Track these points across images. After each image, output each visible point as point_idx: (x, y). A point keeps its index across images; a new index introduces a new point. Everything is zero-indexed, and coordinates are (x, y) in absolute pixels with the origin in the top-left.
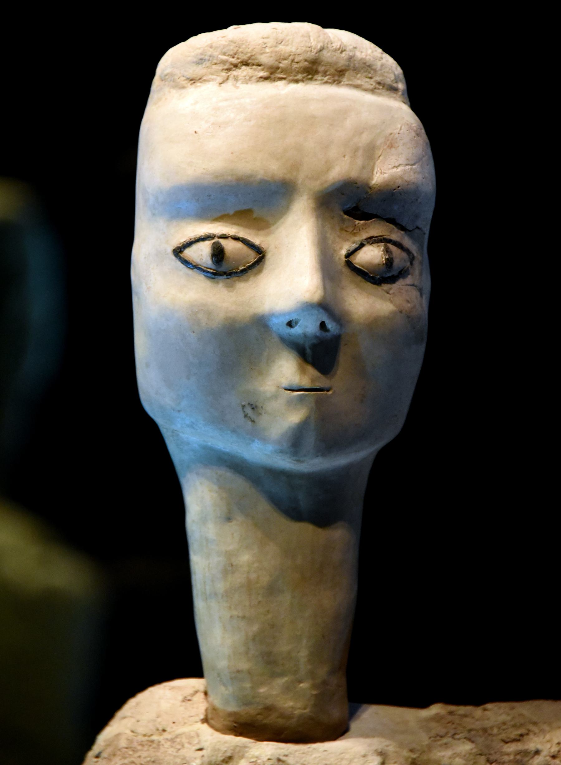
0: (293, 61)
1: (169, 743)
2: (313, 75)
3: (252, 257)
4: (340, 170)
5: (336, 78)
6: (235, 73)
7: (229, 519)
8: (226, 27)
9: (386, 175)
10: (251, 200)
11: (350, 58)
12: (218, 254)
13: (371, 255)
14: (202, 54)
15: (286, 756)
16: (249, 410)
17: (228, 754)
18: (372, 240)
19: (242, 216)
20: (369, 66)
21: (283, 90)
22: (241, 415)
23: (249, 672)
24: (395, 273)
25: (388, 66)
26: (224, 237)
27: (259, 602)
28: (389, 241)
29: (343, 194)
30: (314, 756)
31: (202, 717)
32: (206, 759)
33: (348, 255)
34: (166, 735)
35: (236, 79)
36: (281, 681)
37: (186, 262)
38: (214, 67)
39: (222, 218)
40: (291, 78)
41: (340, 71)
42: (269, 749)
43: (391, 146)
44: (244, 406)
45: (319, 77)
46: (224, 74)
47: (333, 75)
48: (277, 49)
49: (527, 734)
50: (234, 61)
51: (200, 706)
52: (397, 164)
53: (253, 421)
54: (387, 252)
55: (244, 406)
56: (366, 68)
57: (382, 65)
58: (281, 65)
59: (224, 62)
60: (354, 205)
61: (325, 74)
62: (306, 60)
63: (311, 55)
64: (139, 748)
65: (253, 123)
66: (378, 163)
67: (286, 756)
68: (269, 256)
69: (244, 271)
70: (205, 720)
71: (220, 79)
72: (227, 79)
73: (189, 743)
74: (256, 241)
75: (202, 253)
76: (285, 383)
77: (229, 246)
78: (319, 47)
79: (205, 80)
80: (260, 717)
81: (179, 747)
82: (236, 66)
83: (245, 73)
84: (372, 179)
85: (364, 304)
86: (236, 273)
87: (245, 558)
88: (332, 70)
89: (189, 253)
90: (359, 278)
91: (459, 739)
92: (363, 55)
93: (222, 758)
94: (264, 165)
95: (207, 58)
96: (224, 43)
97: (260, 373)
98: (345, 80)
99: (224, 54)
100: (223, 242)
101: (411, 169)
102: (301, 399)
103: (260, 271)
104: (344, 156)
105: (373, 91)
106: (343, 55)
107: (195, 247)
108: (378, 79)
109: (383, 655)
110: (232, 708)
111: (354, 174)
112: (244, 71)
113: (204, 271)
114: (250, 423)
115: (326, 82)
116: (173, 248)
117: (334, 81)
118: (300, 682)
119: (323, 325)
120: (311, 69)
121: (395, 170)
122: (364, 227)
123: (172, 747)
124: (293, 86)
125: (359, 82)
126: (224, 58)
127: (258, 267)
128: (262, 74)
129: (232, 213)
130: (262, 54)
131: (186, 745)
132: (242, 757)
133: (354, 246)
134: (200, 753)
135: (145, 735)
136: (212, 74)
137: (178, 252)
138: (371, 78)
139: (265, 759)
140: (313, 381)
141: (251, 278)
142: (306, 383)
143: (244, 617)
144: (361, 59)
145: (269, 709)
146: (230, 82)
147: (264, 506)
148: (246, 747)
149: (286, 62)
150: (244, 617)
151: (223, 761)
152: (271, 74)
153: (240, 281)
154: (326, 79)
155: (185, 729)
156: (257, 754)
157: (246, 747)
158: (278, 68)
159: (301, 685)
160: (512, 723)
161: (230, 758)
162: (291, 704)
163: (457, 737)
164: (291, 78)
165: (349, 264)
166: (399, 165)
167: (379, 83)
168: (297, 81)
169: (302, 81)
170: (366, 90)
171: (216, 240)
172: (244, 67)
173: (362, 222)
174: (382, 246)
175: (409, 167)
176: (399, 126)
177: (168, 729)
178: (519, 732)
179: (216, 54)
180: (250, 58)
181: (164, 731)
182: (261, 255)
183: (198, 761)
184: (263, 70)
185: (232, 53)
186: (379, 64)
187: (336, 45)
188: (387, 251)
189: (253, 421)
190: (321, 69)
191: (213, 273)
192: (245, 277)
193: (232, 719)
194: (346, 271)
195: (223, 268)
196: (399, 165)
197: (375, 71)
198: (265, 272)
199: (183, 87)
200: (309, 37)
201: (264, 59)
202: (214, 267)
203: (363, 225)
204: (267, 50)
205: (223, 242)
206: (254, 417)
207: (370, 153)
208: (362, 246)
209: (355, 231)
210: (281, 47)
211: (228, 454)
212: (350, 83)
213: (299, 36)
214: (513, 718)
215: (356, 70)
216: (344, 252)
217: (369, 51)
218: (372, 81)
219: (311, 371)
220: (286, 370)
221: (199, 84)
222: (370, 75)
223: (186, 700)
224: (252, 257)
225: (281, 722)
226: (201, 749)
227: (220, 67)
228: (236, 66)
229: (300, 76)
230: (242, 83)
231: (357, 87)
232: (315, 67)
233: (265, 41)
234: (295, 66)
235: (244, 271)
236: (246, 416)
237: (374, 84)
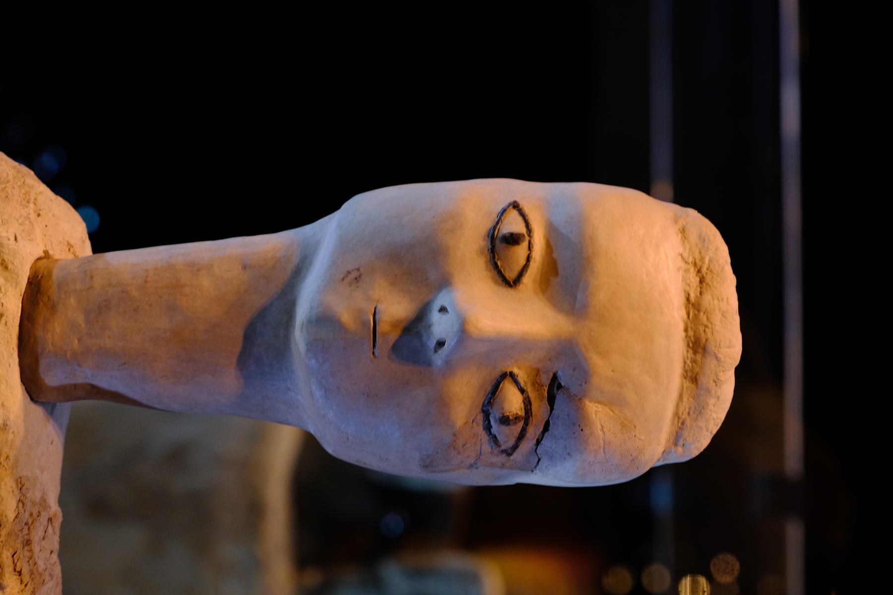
0: (706, 326)
1: (25, 214)
2: (692, 348)
3: (511, 275)
4: (598, 364)
5: (689, 374)
6: (692, 270)
7: (245, 267)
8: (736, 271)
9: (594, 416)
10: (567, 275)
11: (708, 391)
12: (513, 240)
13: (512, 401)
14: (709, 240)
15: (6, 324)
16: (354, 275)
17: (10, 267)
18: (527, 403)
19: (552, 267)
20: (700, 412)
21: (676, 315)
22: (350, 268)
23: (91, 287)
24: (495, 428)
25: (699, 441)
26: (530, 248)
27: (161, 297)
28: (526, 424)
29: (574, 370)
30: (4, 352)
31: (51, 252)
32: (5, 242)
33: (512, 375)
34: (33, 216)
35: (687, 271)
36: (80, 319)
37: (508, 206)
38: (697, 252)
39: (549, 247)
40: (689, 324)
41: (696, 379)
42: (14, 307)
43: (623, 426)
44: (358, 270)
45: (690, 354)
46: (691, 260)
47: (692, 371)
48: (717, 311)
49: (22, 582)
50: (704, 270)
51: (59, 253)
52: (605, 430)
53: (343, 279)
54: (516, 418)
55: (358, 270)
56: (699, 410)
57: (701, 428)
58: (702, 314)
59: (702, 260)
60: (563, 384)
61: (694, 361)
62: (707, 340)
63: (711, 346)
64: (23, 191)
65: (644, 277)
66: (607, 409)
67: (6, 324)
68: (510, 292)
69: (496, 266)
70: (47, 255)
71: (686, 255)
72: (686, 263)
73: (23, 231)
74: (527, 279)
75: (513, 224)
76: (381, 307)
77: (521, 251)
78: (719, 355)
79: (684, 242)
80: (45, 299)
81: (20, 221)
82: (699, 271)
83: (692, 279)
84: (590, 402)
85: (464, 391)
86: (494, 257)
87: (206, 282)
88: (697, 370)
89: (513, 214)
90: (489, 388)
91: (17, 507)
92: (711, 407)
93: (6, 259)
94: (603, 287)
95: (706, 245)
96: (721, 261)
97: (393, 284)
98: (687, 384)
99: (710, 261)
100: (525, 244)
101: (600, 447)
102: (365, 324)
103: (496, 283)
104: (613, 371)
105: (676, 414)
106: (712, 383)
107: (520, 219)
108: (688, 422)
109: (124, 485)
110: (56, 274)
111: (595, 380)
112: (694, 280)
113: (498, 223)
114: (342, 276)
115: (685, 363)
116: (518, 201)
117: (686, 372)
118: (79, 340)
119: (441, 344)
120: (698, 345)
121: (599, 427)
122: (540, 396)
123: (21, 216)
124: (681, 326)
125: (685, 399)
126: (707, 260)
127: (500, 280)
128: (692, 296)
129: (555, 255)
130: (712, 296)
131: (22, 228)
132: (6, 280)
133: (522, 384)
134: (13, 238)
135: (35, 199)
136: (690, 249)
137: (515, 206)
138: (689, 414)
139: (3, 301)
140: (384, 334)
141: (489, 274)
142: (382, 328)
143: (146, 282)
144: (708, 404)
145: (53, 308)
146: (682, 264)
147: (258, 302)
148: (17, 284)
149: (705, 319)
150: (146, 282)
151: (3, 260)
152: (693, 304)
153: (486, 262)
154: (688, 362)
155: (38, 232)
156: (9, 294)
157: (17, 284)
158: (699, 311)
159: (76, 341)
160: (35, 571)
161: (6, 268)
162: (58, 330)
163: (21, 505)
164: (689, 324)
165: (504, 376)
166: (604, 433)
167: (683, 423)
168: (686, 330)
169: (686, 336)
170: (677, 406)
171: (527, 238)
172: (698, 279)
173: (546, 394)
174: (522, 413)
175: (602, 445)
176: (642, 438)
177: (40, 219)
178: (25, 571)
179: (710, 253)
180: (707, 284)
181: (39, 215)
182: (512, 283)
183: (4, 234)
184: (697, 297)
185: (712, 267)
186: (702, 424)
187: (722, 376)
188: (517, 418)
189: (343, 279)
190: (699, 357)
191: (493, 234)
192: (491, 267)
193: (45, 273)
194: (497, 373)
195: (499, 244)
196: (604, 433)
197: (696, 419)
198: (495, 288)
199: (676, 222)
200: (729, 348)
201: (707, 298)
202: (500, 235)
203: (543, 395)
204: (716, 301)
205: (525, 244)
206: (347, 280)
207: (615, 402)
208: (522, 391)
209: (537, 385)
210: (720, 315)
211: (311, 264)
212: (685, 390)
213: (729, 342)
214: (40, 574)
215: (696, 397)
216: (516, 371)
217: (714, 416)
218: (685, 416)
219: (394, 336)
220: (395, 308)
221: (680, 236)
222: (691, 413)
223: (70, 246)
224: (511, 275)
225: (41, 320)
226: (16, 239)
227: (697, 256)
228: (699, 271)
229: (691, 333)
230: (683, 276)
231: (681, 397)
232: (700, 350)
233: (725, 300)
234: (701, 329)
235: (496, 266)
236: (349, 272)
237: (683, 417)
